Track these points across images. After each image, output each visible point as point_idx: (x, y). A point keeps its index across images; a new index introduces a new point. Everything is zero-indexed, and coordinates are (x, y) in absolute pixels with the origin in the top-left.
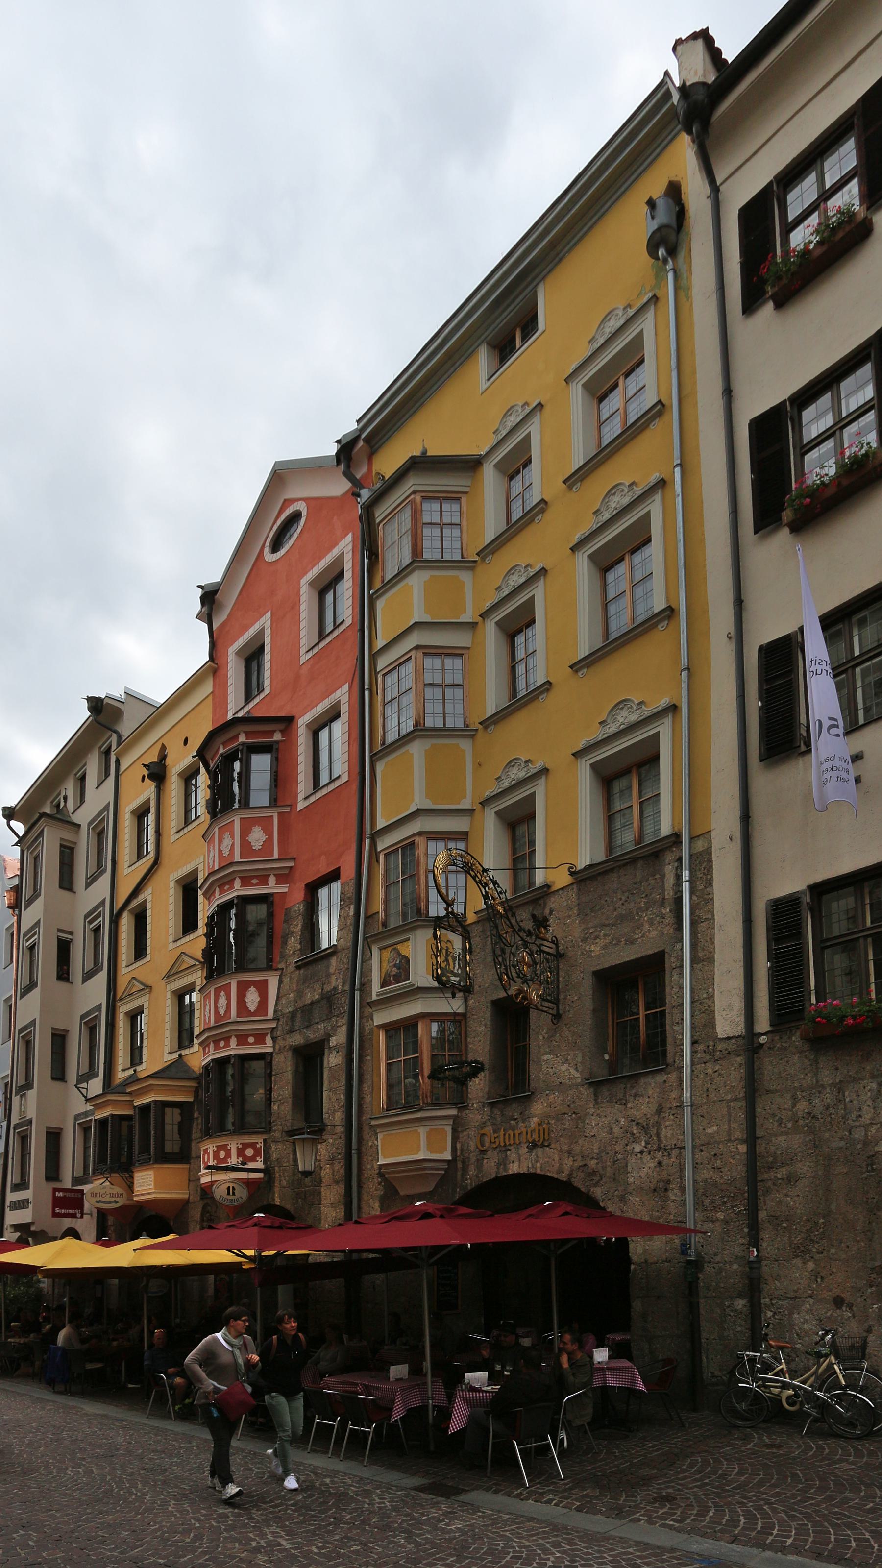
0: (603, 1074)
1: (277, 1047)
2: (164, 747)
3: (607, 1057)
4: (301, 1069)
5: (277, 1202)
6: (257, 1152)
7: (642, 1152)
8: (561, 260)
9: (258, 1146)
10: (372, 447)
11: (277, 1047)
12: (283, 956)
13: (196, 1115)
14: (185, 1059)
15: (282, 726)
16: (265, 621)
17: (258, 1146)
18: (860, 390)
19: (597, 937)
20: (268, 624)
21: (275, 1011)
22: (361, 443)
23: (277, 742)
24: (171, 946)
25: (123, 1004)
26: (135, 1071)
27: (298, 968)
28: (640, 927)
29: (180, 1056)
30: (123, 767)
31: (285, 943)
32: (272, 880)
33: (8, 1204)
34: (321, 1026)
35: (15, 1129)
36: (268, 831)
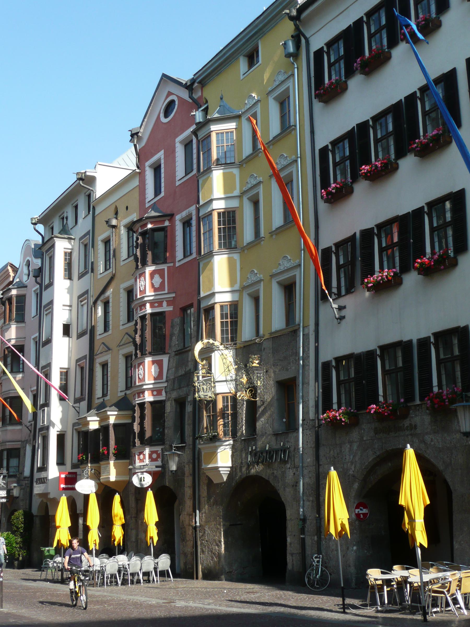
0: (21, 555)
1: (167, 397)
2: (116, 208)
3: (284, 420)
4: (178, 410)
5: (167, 484)
6: (158, 456)
7: (290, 468)
8: (265, 34)
9: (159, 452)
10: (202, 84)
11: (167, 397)
12: (170, 346)
13: (426, 100)
14: (128, 396)
15: (169, 218)
16: (161, 154)
17: (159, 452)
18: (106, 452)
19: (277, 365)
20: (162, 157)
21: (167, 377)
22: (196, 84)
23: (166, 227)
24: (122, 327)
25: (98, 358)
26: (104, 400)
27: (176, 355)
28: (289, 363)
29: (125, 394)
30: (97, 213)
31: (171, 339)
32: (165, 304)
33: (35, 480)
34: (185, 389)
35: (39, 432)
36: (162, 277)
